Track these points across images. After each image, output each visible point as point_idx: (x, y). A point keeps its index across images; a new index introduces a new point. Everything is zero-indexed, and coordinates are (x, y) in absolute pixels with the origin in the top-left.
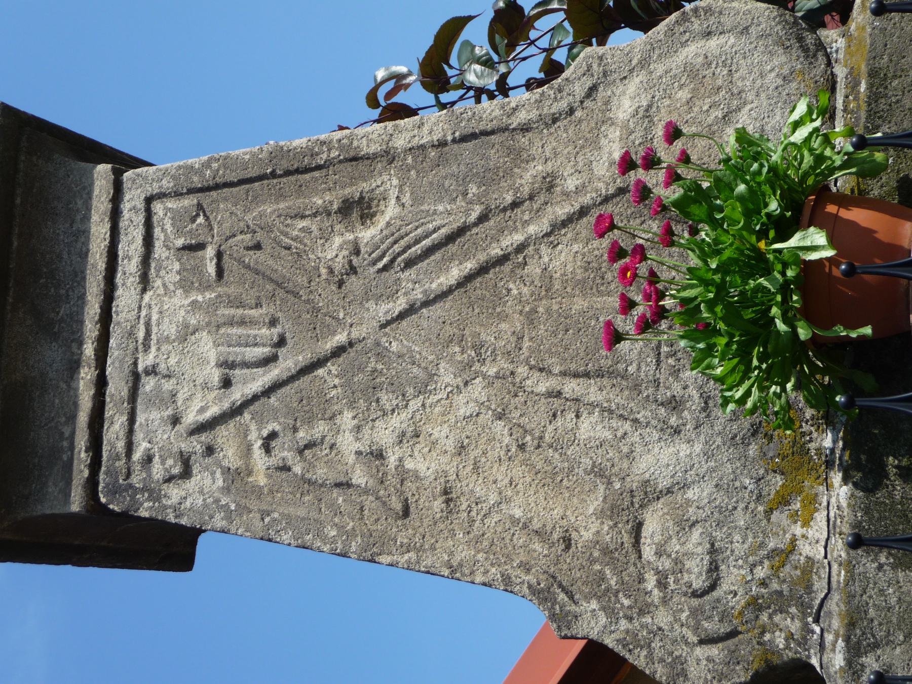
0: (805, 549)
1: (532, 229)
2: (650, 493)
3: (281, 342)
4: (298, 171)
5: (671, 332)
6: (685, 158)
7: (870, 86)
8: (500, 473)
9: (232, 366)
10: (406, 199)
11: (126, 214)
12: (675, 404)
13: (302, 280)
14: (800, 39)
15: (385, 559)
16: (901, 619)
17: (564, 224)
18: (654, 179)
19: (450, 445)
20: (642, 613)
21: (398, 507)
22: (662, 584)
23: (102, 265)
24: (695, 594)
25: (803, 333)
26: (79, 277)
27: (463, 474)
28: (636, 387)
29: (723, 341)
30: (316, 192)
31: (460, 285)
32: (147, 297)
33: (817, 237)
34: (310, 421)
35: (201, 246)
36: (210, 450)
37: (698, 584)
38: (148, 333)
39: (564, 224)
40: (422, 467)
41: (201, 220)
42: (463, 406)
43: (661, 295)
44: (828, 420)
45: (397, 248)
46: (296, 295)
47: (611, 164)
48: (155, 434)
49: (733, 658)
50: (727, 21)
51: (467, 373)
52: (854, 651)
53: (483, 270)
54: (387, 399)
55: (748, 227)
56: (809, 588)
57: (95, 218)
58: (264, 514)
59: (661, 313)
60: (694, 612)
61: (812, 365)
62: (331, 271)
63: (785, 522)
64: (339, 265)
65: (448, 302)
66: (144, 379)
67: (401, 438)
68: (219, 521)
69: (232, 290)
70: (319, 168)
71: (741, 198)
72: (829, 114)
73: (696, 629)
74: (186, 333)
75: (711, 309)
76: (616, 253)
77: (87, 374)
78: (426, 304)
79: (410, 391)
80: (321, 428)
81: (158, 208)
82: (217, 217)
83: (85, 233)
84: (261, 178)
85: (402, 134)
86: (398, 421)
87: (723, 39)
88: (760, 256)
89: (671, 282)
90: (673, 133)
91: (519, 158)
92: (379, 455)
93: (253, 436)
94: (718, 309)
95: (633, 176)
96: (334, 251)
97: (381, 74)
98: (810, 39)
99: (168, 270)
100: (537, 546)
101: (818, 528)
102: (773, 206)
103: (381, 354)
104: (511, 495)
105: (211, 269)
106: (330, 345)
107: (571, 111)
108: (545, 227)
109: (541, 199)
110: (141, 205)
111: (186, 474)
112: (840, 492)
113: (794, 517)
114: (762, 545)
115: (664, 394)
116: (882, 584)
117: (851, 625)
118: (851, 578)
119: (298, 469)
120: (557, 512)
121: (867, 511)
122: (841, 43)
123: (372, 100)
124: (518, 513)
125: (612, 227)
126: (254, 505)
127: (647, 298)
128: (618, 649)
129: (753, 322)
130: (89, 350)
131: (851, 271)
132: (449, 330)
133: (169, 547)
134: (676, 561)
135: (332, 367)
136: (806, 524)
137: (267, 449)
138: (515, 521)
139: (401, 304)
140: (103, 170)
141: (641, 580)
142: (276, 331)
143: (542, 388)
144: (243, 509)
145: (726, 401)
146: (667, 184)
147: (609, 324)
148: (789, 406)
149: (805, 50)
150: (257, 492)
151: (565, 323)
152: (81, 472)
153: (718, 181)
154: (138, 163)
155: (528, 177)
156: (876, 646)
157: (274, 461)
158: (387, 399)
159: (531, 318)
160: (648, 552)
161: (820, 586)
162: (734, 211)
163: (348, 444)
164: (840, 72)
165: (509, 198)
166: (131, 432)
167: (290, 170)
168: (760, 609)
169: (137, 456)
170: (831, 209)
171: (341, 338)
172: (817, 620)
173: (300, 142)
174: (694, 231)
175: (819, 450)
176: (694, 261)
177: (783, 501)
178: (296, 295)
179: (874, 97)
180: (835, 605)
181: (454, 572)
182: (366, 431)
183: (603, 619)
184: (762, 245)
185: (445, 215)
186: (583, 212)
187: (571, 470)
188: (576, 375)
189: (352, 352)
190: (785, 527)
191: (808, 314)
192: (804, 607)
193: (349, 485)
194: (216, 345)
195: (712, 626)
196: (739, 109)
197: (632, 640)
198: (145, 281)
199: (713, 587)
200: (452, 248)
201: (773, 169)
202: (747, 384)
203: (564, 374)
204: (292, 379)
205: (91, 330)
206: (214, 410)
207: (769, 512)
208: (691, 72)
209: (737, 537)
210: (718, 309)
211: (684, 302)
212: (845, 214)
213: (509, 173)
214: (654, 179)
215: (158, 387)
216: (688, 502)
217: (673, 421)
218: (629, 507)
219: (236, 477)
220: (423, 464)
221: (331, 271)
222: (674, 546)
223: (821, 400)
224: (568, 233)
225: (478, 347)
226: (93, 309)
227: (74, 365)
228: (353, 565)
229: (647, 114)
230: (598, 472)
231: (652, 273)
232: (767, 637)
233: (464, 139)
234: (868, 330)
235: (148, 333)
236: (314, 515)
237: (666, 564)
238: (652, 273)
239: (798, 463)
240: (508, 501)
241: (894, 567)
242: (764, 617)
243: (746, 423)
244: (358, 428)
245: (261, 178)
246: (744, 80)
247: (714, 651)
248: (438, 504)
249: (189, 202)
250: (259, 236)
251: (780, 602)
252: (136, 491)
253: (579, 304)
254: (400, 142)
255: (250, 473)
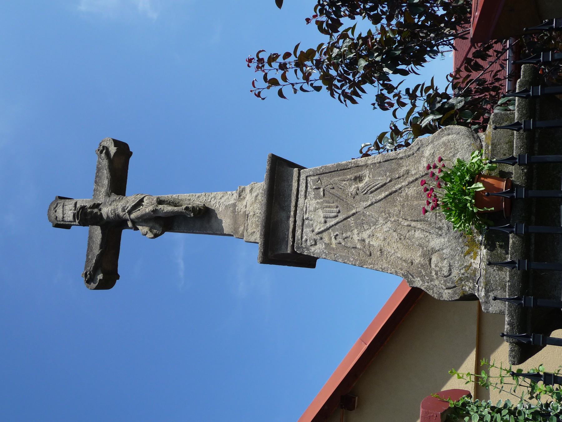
0: (474, 265)
1: (403, 184)
2: (433, 251)
3: (339, 212)
4: (343, 170)
5: (440, 210)
6: (444, 166)
7: (492, 147)
8: (395, 245)
9: (327, 218)
10: (371, 176)
11: (301, 180)
12: (440, 228)
13: (344, 197)
14: (473, 135)
15: (365, 266)
16: (500, 284)
17: (411, 182)
18: (436, 171)
19: (382, 238)
20: (431, 281)
21: (369, 253)
22: (436, 274)
23: (295, 193)
24: (445, 277)
25: (475, 210)
26: (290, 196)
27: (385, 245)
28: (430, 224)
29: (454, 212)
30: (348, 175)
31: (384, 198)
32: (306, 201)
33: (480, 185)
34: (346, 232)
35: (319, 188)
36: (321, 239)
37: (446, 274)
38: (306, 210)
39: (411, 182)
40: (374, 244)
41: (319, 182)
42: (385, 228)
43: (437, 201)
44: (481, 233)
45: (368, 189)
46: (343, 200)
47: (424, 167)
48: (308, 234)
49: (455, 293)
50: (454, 131)
51: (386, 220)
52: (487, 292)
53: (390, 194)
54: (366, 227)
55: (461, 183)
56: (475, 276)
57: (294, 181)
58: (335, 254)
59: (437, 205)
60: (445, 281)
61: (477, 218)
62: (352, 194)
63: (469, 259)
64: (354, 193)
65: (382, 202)
66: (305, 221)
67: (369, 236)
68: (324, 256)
69: (327, 199)
70: (349, 169)
71: (459, 176)
72: (481, 155)
73: (445, 285)
74: (316, 210)
75: (451, 204)
76: (426, 190)
77: (292, 219)
78: (376, 203)
79: (372, 224)
80: (349, 234)
81: (309, 179)
82: (323, 181)
83: (291, 185)
84: (334, 171)
85: (370, 160)
86: (368, 232)
87: (453, 136)
88: (464, 191)
89: (440, 197)
90: (441, 160)
91: (400, 166)
92: (364, 240)
93: (332, 235)
94: (453, 204)
95: (430, 171)
96: (352, 189)
97: (363, 145)
98: (475, 135)
99: (311, 194)
100: (404, 264)
101: (478, 260)
102: (467, 178)
103: (364, 215)
104: (398, 251)
105: (322, 194)
106: (351, 213)
107: (413, 154)
108: (407, 183)
109: (405, 176)
110: (305, 178)
111: (316, 244)
112: (484, 251)
113: (471, 257)
114: (463, 264)
115: (438, 226)
116: (495, 275)
117: (486, 285)
118: (486, 273)
119: (343, 244)
120: (409, 256)
121: (491, 256)
122: (484, 136)
123: (361, 152)
124: (399, 256)
125: (425, 183)
126: (332, 252)
127: (434, 201)
128: (425, 290)
129: (462, 207)
130: (292, 213)
131: (488, 195)
132: (382, 209)
133: (309, 262)
134: (440, 268)
135: (352, 218)
136: (474, 259)
137: (335, 238)
138: (398, 258)
139: (369, 203)
140: (296, 170)
141: (431, 273)
142: (338, 209)
143: (406, 224)
144: (329, 253)
145: (454, 228)
146: (439, 172)
147: (424, 208)
148: (470, 229)
149: (474, 138)
150: (333, 249)
151: (411, 208)
152: (290, 243)
153: (453, 171)
154: (304, 168)
155: (402, 170)
156: (493, 290)
157: (337, 241)
158: (366, 227)
159: (403, 206)
160: (433, 266)
161: (478, 275)
162: (457, 179)
163: (356, 238)
164: (484, 144)
165: (397, 176)
166: (302, 234)
167: (342, 169)
168: (462, 280)
169: (304, 240)
170: (482, 179)
171: (354, 211)
172: (477, 284)
173: (344, 162)
174: (446, 184)
175: (478, 241)
176: (446, 192)
177: (468, 253)
178: (343, 200)
179: (493, 150)
180: (482, 280)
181: (383, 270)
182: (360, 234)
183: (421, 283)
184: (464, 188)
185: (381, 180)
186: (416, 179)
187: (413, 245)
188: (414, 221)
189: (357, 215)
190: (469, 260)
191: (476, 205)
192: (474, 280)
193: (356, 248)
194: (323, 212)
195: (449, 285)
196: (457, 153)
197: (428, 288)
198: (306, 197)
199: (450, 275)
200: (382, 188)
201: (467, 169)
202: (460, 223)
203: (411, 220)
204: (342, 221)
205: (293, 209)
206: (322, 229)
207: (465, 256)
208: (445, 144)
209: (456, 262)
210: (453, 204)
211: (444, 202)
212: (486, 180)
213: (397, 170)
214: (436, 171)
215: (309, 223)
216: (444, 254)
217: (440, 233)
218: (428, 255)
219: (328, 245)
220: (374, 243)
221: (352, 194)
222: (440, 265)
223: (479, 228)
224: (413, 185)
225: (389, 214)
226: (293, 204)
227: (289, 217)
228: (357, 267)
229: (433, 155)
230: (420, 245)
231: (435, 195)
232: (464, 288)
233: (386, 161)
234: (493, 209)
235: (306, 210)
236: (347, 255)
237: (438, 269)
238: (435, 195)
239: (472, 244)
240: (397, 252)
241: (498, 270)
242: (463, 283)
243: (459, 233)
244: (358, 234)
245: (334, 171)
246: (458, 146)
247: (450, 291)
248: (379, 253)
249: (316, 177)
250: (334, 186)
251: (467, 279)
252: (303, 248)
253: (416, 203)
254: (369, 162)
255: (331, 244)
